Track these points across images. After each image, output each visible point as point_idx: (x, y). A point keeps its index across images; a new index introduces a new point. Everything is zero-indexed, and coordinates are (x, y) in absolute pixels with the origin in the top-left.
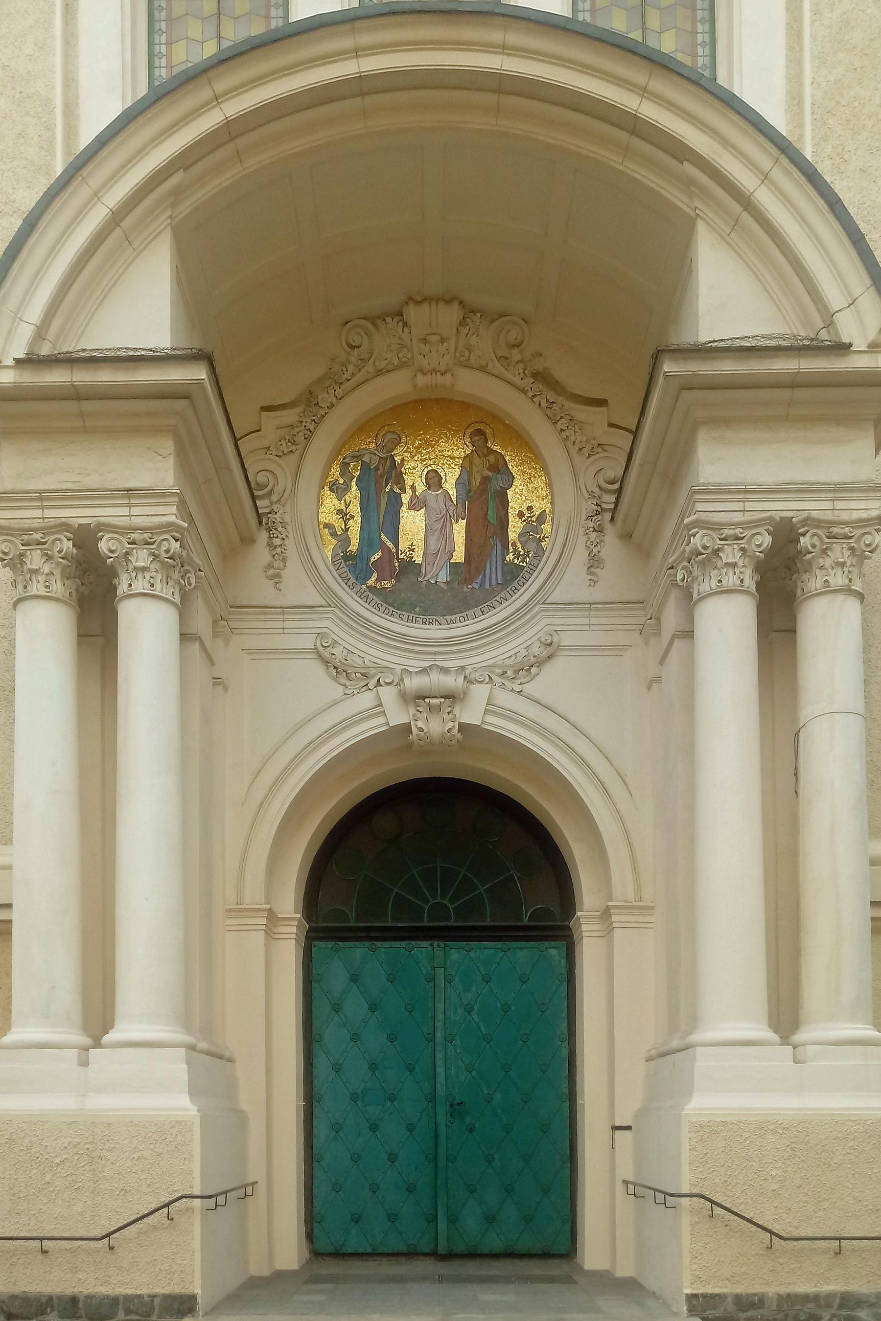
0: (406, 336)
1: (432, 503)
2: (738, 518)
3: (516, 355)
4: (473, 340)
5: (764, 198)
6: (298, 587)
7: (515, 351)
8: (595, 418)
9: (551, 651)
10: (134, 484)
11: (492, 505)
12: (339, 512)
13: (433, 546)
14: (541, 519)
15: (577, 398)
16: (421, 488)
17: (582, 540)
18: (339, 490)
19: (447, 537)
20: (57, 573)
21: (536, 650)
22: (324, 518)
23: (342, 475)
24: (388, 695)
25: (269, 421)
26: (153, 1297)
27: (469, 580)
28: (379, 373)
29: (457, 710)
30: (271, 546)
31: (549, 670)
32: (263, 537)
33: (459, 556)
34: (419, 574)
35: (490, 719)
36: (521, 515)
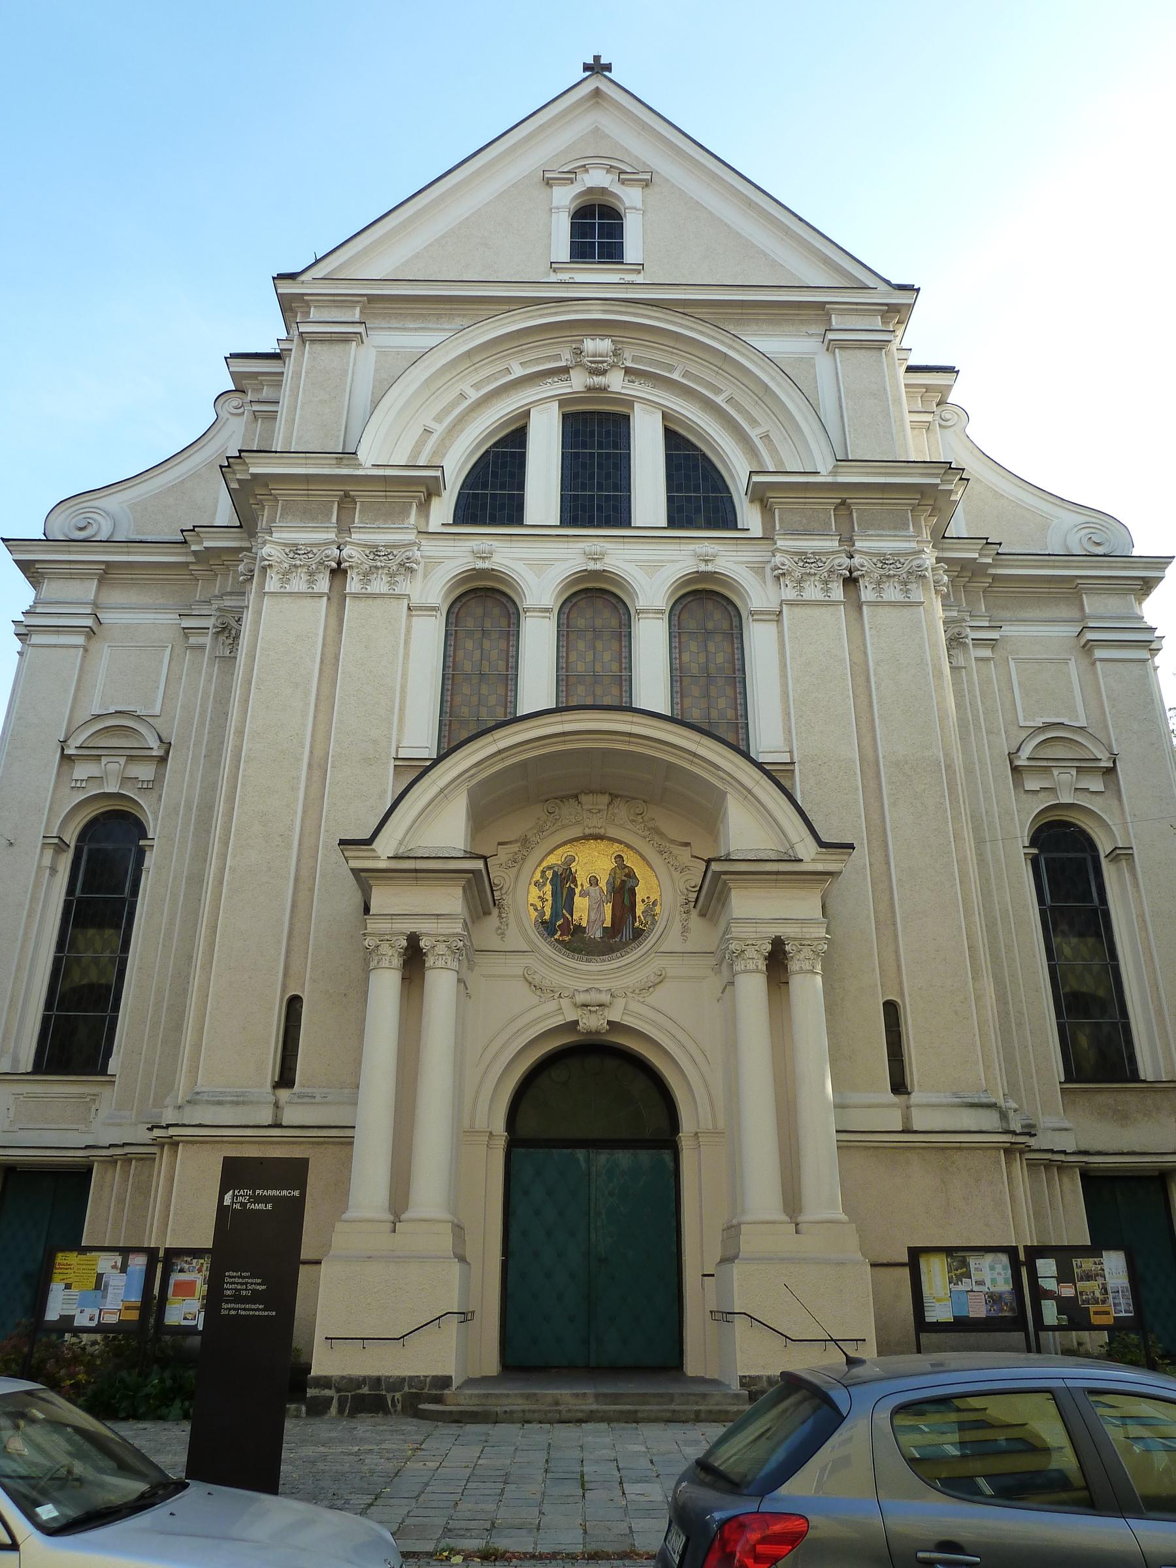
1: (592, 894)
2: (753, 936)
5: (757, 791)
6: (513, 940)
8: (684, 855)
9: (661, 979)
14: (654, 904)
15: (672, 841)
16: (587, 885)
17: (678, 918)
21: (652, 978)
22: (531, 901)
24: (565, 1003)
26: (426, 1377)
28: (564, 827)
29: (606, 1014)
30: (500, 916)
32: (495, 912)
33: (608, 923)
35: (625, 1017)
36: (643, 901)
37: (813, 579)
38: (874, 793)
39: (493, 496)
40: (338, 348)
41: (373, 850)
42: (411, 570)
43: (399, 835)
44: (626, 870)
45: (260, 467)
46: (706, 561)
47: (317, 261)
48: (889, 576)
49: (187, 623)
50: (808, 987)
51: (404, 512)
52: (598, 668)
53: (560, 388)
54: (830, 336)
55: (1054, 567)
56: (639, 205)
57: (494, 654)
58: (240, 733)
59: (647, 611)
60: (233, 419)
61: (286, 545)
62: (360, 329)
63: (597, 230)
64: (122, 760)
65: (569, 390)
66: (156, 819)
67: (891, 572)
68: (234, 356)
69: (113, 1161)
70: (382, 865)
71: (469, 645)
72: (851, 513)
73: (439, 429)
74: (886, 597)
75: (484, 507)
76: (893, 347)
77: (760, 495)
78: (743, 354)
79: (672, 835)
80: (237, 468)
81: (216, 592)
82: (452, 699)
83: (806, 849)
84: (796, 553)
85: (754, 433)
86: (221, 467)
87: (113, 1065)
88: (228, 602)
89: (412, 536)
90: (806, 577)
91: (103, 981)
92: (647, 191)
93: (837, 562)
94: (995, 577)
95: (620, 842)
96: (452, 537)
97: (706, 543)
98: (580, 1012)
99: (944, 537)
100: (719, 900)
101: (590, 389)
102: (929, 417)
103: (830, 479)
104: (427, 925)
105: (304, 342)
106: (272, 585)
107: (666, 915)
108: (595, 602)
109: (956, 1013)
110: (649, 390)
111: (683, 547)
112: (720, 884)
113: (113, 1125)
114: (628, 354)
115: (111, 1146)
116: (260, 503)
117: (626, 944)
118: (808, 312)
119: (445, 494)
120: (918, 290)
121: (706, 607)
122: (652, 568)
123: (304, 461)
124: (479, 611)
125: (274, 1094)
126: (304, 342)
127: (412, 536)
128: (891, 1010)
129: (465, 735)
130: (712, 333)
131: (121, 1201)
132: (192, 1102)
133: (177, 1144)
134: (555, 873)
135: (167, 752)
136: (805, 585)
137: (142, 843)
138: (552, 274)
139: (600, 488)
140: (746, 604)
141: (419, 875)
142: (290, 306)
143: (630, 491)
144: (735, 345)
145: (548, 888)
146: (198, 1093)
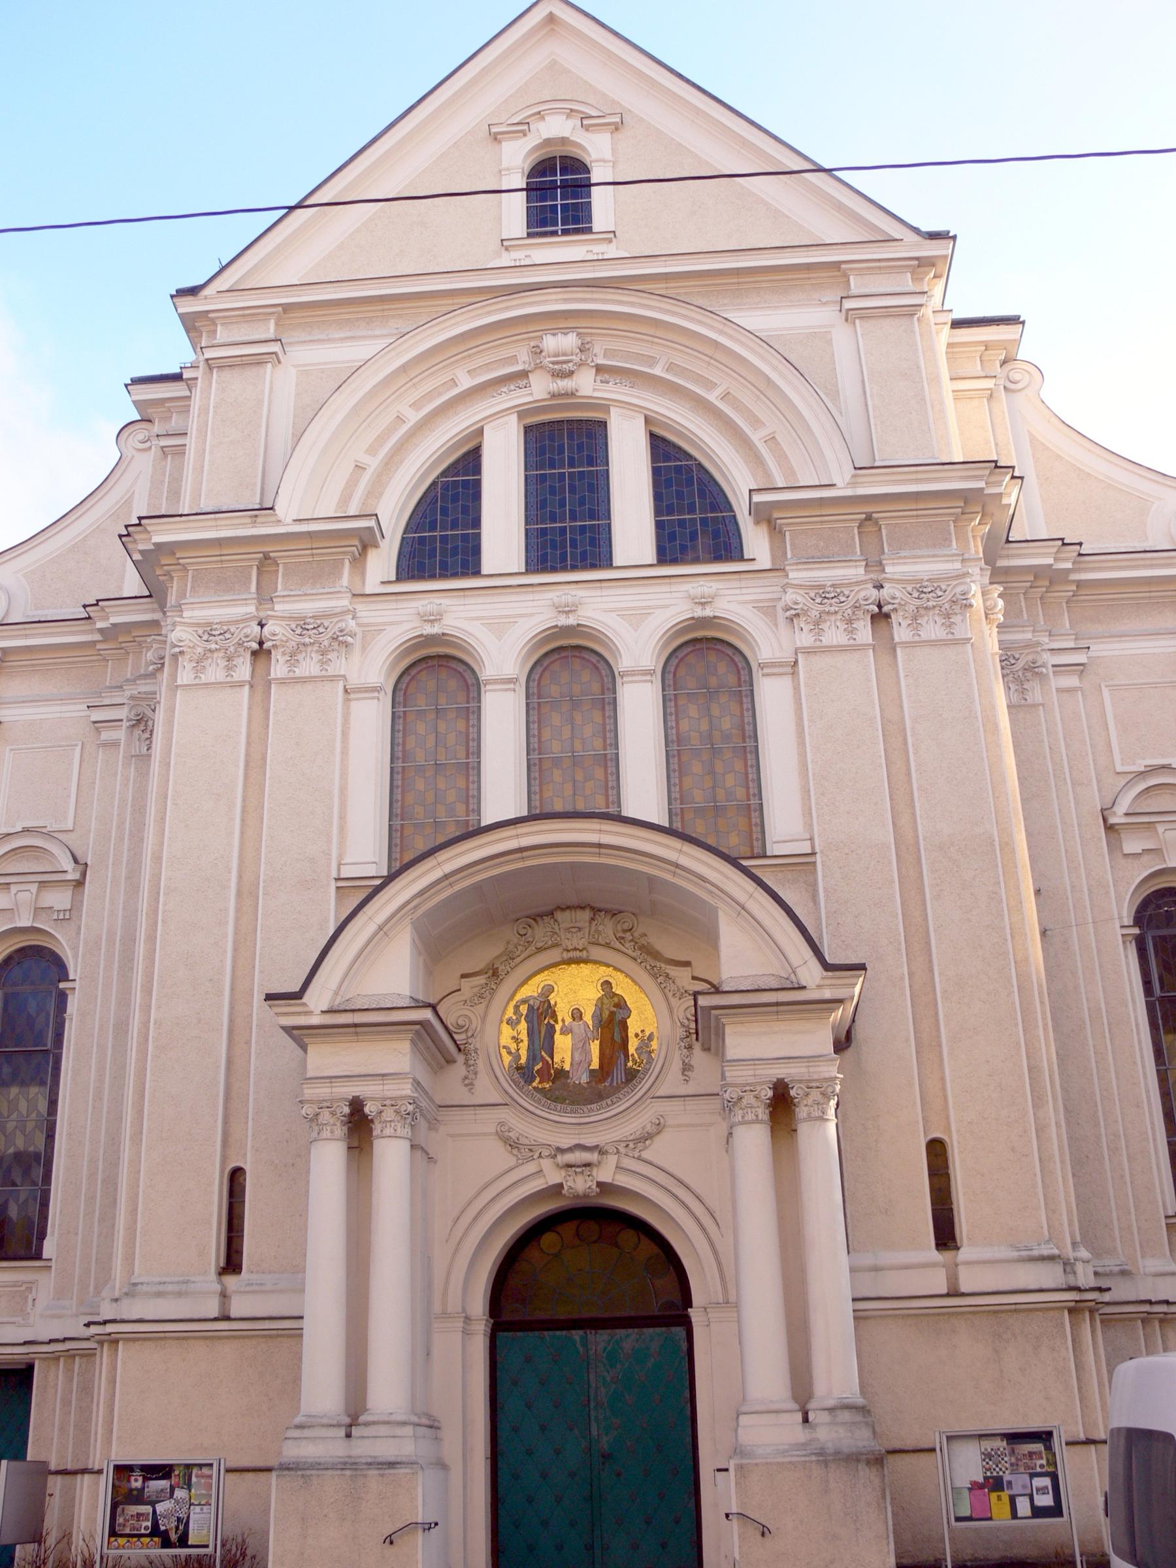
0: (556, 927)
1: (576, 1029)
2: (751, 1080)
3: (628, 936)
4: (601, 928)
5: (751, 906)
6: (485, 1090)
7: (628, 934)
9: (660, 1127)
10: (386, 1068)
11: (616, 1029)
12: (513, 1038)
13: (577, 1056)
14: (650, 1038)
16: (568, 1020)
17: (677, 1053)
18: (512, 1023)
19: (588, 1053)
20: (338, 1124)
22: (503, 1042)
23: (515, 1013)
25: (466, 984)
27: (602, 1080)
28: (539, 950)
30: (466, 1063)
31: (658, 1140)
33: (595, 1065)
34: (568, 1077)
37: (833, 618)
38: (912, 886)
39: (444, 539)
40: (251, 372)
41: (304, 1004)
42: (347, 645)
43: (333, 985)
44: (616, 999)
45: (163, 534)
46: (703, 604)
47: (223, 269)
48: (926, 608)
49: (98, 715)
50: (821, 1136)
51: (335, 569)
52: (578, 745)
53: (518, 397)
54: (848, 304)
55: (1152, 566)
56: (608, 155)
57: (451, 739)
58: (158, 859)
59: (632, 673)
60: (138, 455)
61: (198, 625)
62: (275, 347)
63: (559, 192)
64: (34, 888)
65: (530, 399)
66: (76, 956)
67: (930, 604)
68: (137, 381)
69: (55, 1358)
70: (315, 1020)
71: (421, 728)
72: (880, 529)
73: (373, 463)
74: (924, 635)
75: (432, 554)
76: (927, 311)
77: (764, 515)
78: (737, 340)
79: (670, 952)
80: (137, 537)
81: (129, 676)
82: (403, 797)
83: (811, 973)
84: (812, 587)
85: (756, 437)
86: (120, 536)
87: (49, 1247)
88: (144, 687)
89: (344, 602)
90: (824, 616)
91: (31, 1149)
92: (618, 135)
93: (862, 595)
94: (1079, 584)
95: (608, 966)
96: (393, 597)
97: (702, 581)
98: (563, 1173)
99: (1008, 541)
100: (717, 1034)
101: (554, 396)
102: (989, 384)
103: (849, 492)
104: (372, 1088)
105: (211, 369)
106: (185, 676)
107: (663, 1053)
108: (570, 665)
109: (1013, 1150)
110: (627, 390)
111: (675, 588)
112: (713, 1024)
113: (53, 1316)
114: (598, 349)
115: (51, 1341)
116: (168, 574)
117: (618, 1089)
118: (820, 274)
119: (384, 544)
120: (954, 238)
121: (705, 660)
122: (636, 617)
123: (213, 523)
124: (431, 685)
125: (220, 1282)
126: (211, 369)
127: (344, 602)
128: (937, 1151)
129: (421, 846)
130: (699, 317)
131: (66, 1402)
132: (132, 1290)
133: (116, 1341)
134: (531, 1009)
135: (84, 874)
136: (824, 626)
137: (62, 985)
138: (505, 254)
139: (573, 518)
140: (754, 653)
141: (359, 1029)
142: (192, 324)
143: (609, 518)
144: (726, 329)
145: (523, 1026)
146: (135, 1284)
